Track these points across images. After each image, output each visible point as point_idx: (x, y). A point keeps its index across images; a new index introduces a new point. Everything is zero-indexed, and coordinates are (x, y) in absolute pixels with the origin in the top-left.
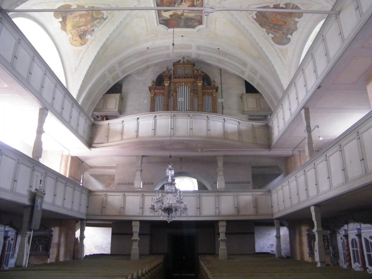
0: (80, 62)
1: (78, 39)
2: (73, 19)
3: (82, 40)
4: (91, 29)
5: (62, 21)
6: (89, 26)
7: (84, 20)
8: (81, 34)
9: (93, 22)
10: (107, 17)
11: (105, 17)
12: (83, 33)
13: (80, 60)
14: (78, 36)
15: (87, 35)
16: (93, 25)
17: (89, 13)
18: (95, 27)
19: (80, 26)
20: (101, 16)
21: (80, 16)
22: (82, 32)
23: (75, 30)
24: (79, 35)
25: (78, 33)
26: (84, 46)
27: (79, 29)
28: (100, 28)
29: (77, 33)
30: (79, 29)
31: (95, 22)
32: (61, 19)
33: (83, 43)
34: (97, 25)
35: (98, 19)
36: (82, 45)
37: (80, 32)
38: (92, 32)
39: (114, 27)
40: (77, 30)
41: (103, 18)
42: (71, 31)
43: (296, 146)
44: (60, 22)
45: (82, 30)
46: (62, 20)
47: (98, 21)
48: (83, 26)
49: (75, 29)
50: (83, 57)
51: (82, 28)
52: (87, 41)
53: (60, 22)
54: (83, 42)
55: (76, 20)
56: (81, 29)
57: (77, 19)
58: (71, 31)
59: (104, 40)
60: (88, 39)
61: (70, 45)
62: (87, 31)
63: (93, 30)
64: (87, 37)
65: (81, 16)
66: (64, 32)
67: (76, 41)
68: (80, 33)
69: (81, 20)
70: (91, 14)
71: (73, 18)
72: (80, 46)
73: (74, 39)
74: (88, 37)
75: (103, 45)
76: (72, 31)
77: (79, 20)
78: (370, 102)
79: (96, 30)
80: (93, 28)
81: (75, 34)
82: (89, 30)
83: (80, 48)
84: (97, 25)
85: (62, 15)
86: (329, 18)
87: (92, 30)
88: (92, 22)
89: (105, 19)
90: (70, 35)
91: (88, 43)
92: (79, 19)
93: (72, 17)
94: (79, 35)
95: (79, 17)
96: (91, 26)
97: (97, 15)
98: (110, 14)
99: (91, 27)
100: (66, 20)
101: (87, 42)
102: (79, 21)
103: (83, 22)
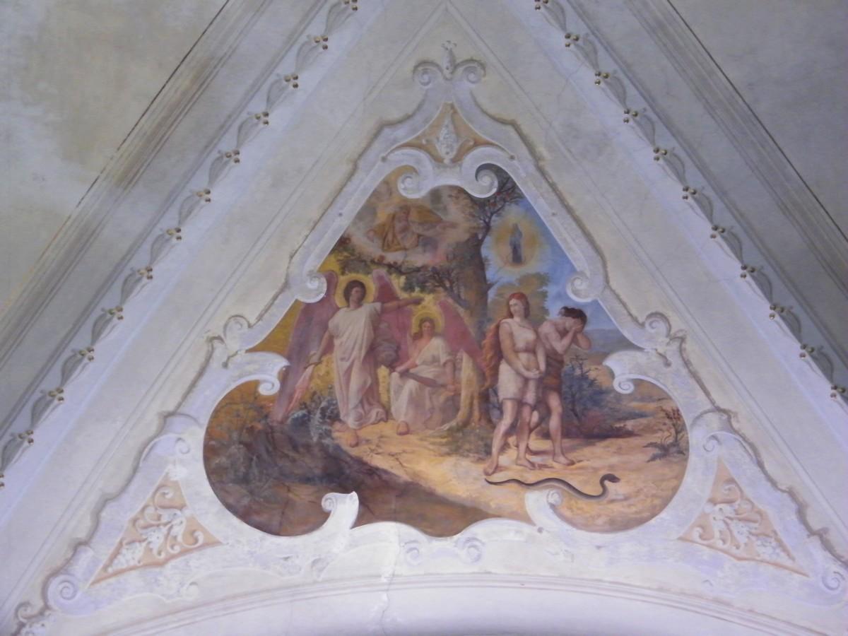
0: (827, 546)
1: (600, 456)
2: (387, 415)
3: (630, 434)
4: (546, 328)
5: (363, 502)
6: (518, 331)
7: (431, 352)
8: (563, 417)
9: (491, 294)
10: (498, 171)
11: (484, 188)
12: (562, 397)
13: (812, 533)
14: (567, 443)
15: (602, 380)
16: (521, 296)
17: (386, 293)
18: (552, 290)
19: (487, 399)
20: (455, 213)
21: (377, 365)
22: (554, 402)
23: (504, 447)
24: (566, 434)
25: (546, 435)
26: (696, 437)
27: (509, 408)
28: (577, 253)
29: (536, 443)
30: (509, 408)
31: (499, 270)
32: (345, 506)
33: (656, 438)
34: (534, 265)
35: (475, 244)
36: (673, 450)
37: (546, 414)
38: (588, 328)
39: (636, 153)
40: (513, 429)
41: (482, 207)
42: (498, 477)
43: (508, 484)
44: (367, 515)
45: (530, 397)
46: (354, 495)
47: (494, 253)
48: (488, 377)
49: (496, 444)
50: (792, 494)
51: (508, 383)
52: (664, 397)
53: (367, 515)
54: (650, 429)
55: (401, 407)
56: (520, 403)
57: (401, 394)
58: (498, 477)
59: (724, 263)
60: (638, 383)
61: (626, 541)
62: (554, 360)
63: (576, 313)
64: (622, 384)
65: (384, 351)
66: (478, 530)
67: (613, 479)
68: (554, 423)
69: (428, 372)
70: (398, 282)
71: (375, 412)
72: (680, 477)
73: (593, 489)
74: (622, 372)
75: (767, 288)
76: (498, 468)
77: (411, 384)
78: (371, 327)
79: (581, 293)
80: (554, 310)
81: (548, 460)
82: (560, 345)
83: (696, 479)
84: (534, 265)
85: (307, 480)
86: (317, 9)
87: (569, 322)
88: (483, 295)
89: (508, 190)
90: (537, 501)
91: (682, 396)
92: (405, 374)
93: (362, 421)
94: (566, 434)
95: (383, 371)
96: (527, 314)
97: (427, 243)
98: (478, 143)
99: (532, 316)
100: (373, 471)
101: (668, 406)
102: (424, 382)
103: (456, 368)
